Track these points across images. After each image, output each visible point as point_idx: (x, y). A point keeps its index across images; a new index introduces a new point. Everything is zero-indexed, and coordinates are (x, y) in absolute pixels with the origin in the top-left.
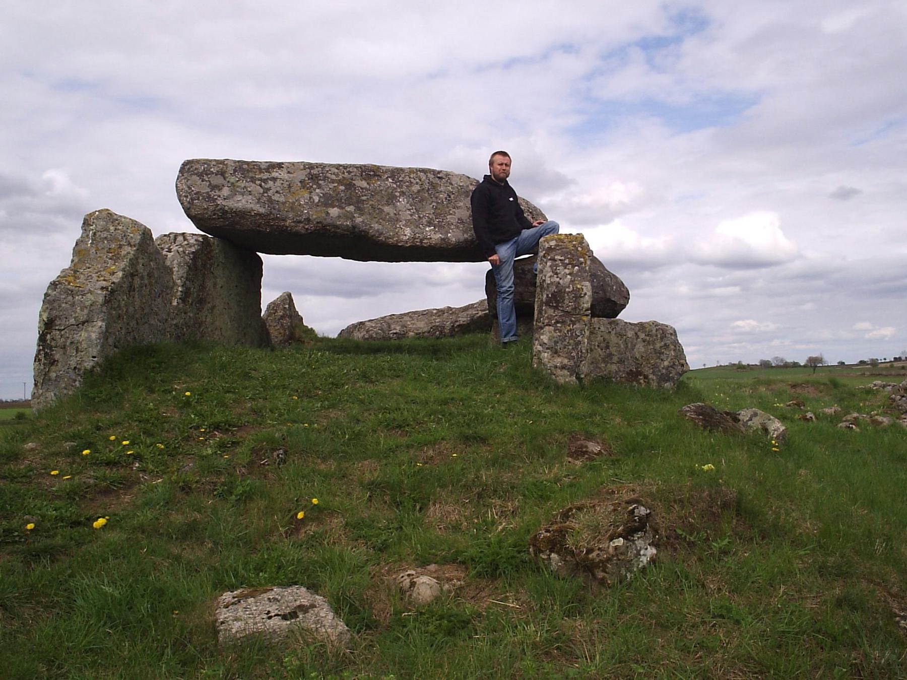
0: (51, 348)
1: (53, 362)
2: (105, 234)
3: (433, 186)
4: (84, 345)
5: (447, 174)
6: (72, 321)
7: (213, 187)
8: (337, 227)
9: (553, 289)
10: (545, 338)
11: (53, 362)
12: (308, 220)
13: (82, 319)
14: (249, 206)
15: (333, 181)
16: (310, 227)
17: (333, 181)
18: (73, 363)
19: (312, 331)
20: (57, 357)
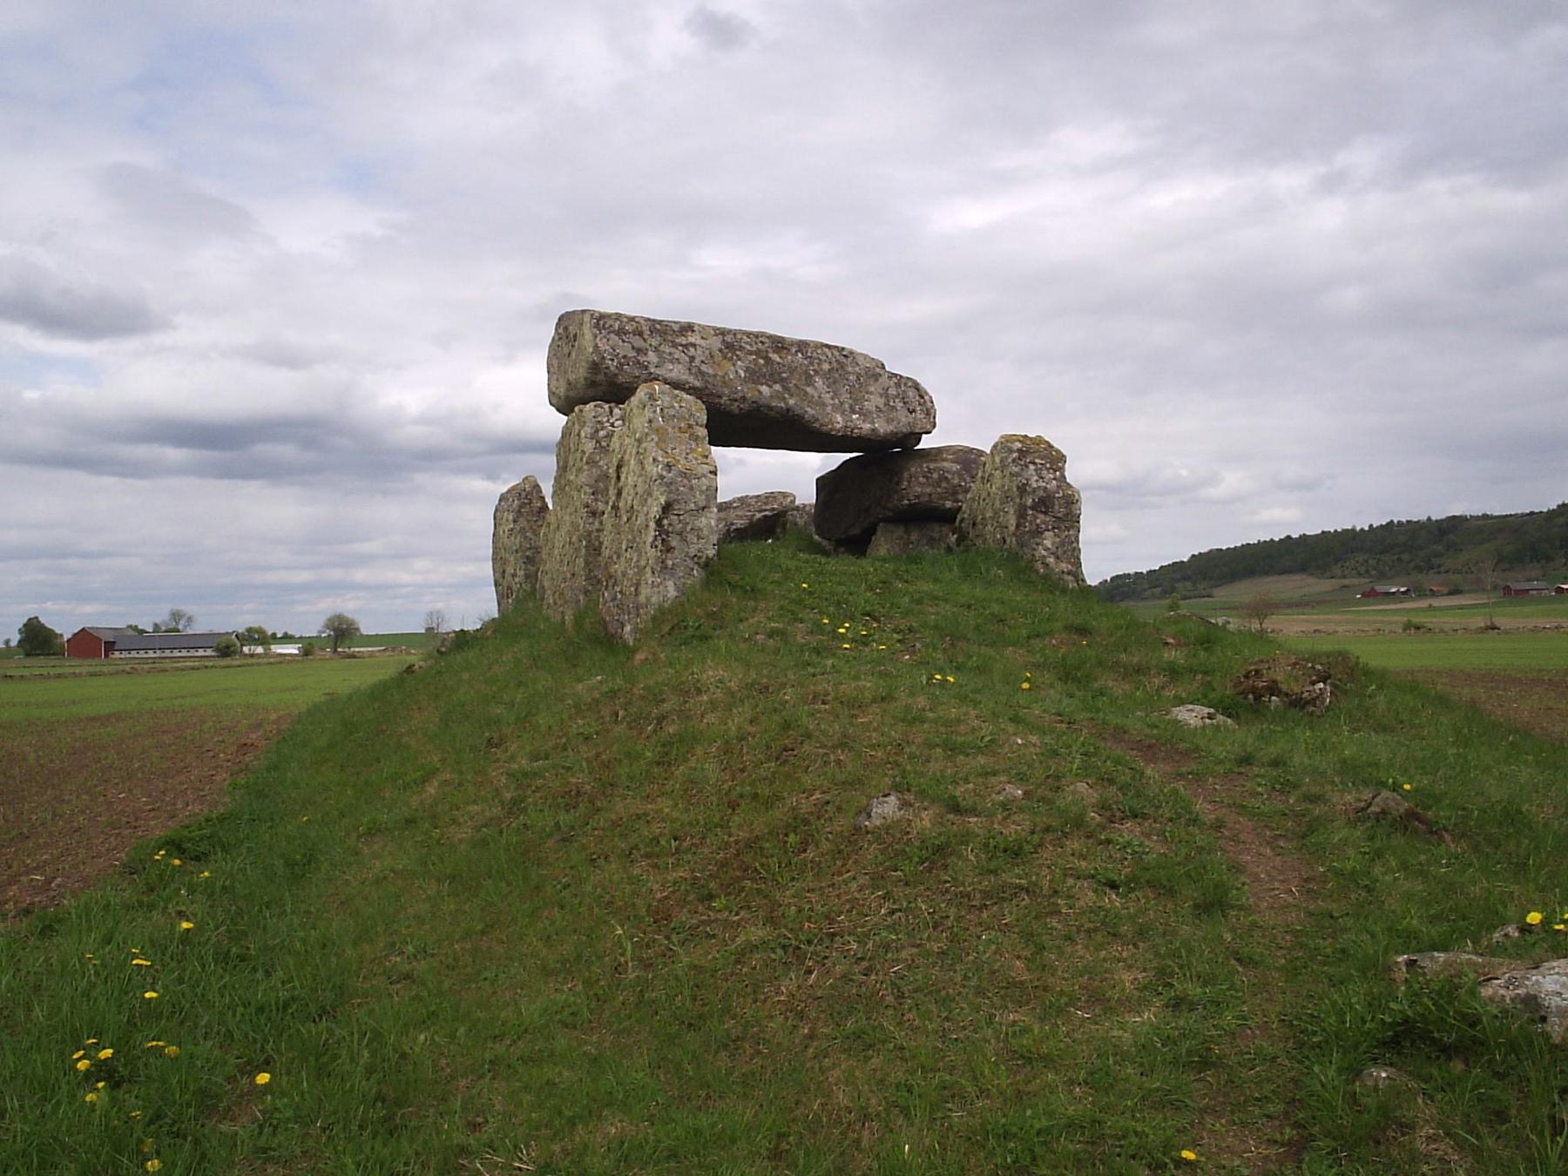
0: (667, 533)
1: (669, 549)
2: (672, 412)
3: (842, 366)
4: (705, 532)
5: (852, 353)
6: (692, 506)
7: (639, 351)
8: (770, 408)
9: (1042, 493)
10: (1048, 543)
11: (669, 549)
12: (744, 398)
13: (701, 504)
14: (684, 377)
15: (751, 353)
16: (745, 406)
17: (751, 353)
18: (693, 551)
19: (1304, 537)
20: (674, 544)
